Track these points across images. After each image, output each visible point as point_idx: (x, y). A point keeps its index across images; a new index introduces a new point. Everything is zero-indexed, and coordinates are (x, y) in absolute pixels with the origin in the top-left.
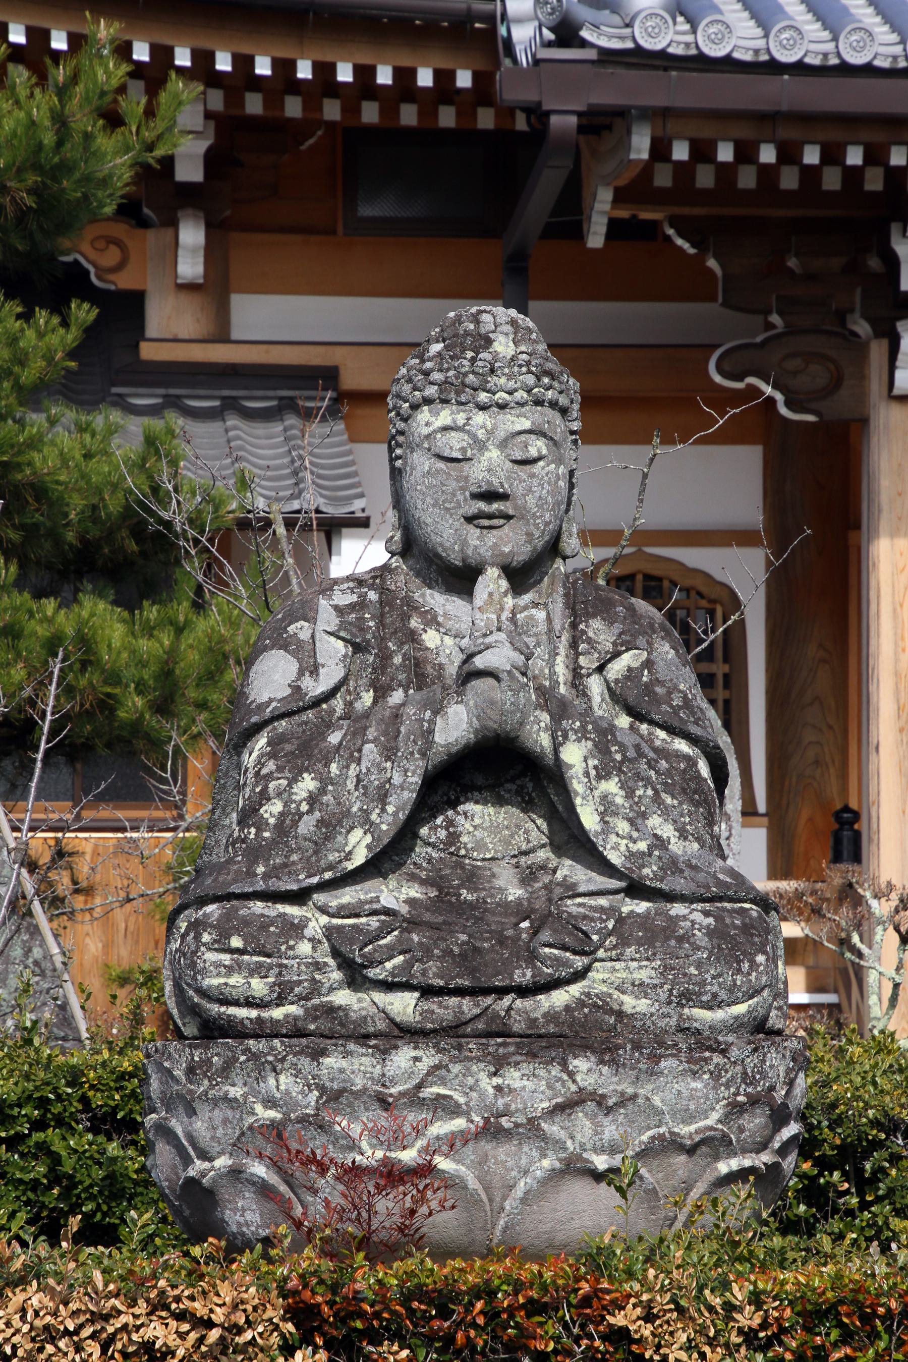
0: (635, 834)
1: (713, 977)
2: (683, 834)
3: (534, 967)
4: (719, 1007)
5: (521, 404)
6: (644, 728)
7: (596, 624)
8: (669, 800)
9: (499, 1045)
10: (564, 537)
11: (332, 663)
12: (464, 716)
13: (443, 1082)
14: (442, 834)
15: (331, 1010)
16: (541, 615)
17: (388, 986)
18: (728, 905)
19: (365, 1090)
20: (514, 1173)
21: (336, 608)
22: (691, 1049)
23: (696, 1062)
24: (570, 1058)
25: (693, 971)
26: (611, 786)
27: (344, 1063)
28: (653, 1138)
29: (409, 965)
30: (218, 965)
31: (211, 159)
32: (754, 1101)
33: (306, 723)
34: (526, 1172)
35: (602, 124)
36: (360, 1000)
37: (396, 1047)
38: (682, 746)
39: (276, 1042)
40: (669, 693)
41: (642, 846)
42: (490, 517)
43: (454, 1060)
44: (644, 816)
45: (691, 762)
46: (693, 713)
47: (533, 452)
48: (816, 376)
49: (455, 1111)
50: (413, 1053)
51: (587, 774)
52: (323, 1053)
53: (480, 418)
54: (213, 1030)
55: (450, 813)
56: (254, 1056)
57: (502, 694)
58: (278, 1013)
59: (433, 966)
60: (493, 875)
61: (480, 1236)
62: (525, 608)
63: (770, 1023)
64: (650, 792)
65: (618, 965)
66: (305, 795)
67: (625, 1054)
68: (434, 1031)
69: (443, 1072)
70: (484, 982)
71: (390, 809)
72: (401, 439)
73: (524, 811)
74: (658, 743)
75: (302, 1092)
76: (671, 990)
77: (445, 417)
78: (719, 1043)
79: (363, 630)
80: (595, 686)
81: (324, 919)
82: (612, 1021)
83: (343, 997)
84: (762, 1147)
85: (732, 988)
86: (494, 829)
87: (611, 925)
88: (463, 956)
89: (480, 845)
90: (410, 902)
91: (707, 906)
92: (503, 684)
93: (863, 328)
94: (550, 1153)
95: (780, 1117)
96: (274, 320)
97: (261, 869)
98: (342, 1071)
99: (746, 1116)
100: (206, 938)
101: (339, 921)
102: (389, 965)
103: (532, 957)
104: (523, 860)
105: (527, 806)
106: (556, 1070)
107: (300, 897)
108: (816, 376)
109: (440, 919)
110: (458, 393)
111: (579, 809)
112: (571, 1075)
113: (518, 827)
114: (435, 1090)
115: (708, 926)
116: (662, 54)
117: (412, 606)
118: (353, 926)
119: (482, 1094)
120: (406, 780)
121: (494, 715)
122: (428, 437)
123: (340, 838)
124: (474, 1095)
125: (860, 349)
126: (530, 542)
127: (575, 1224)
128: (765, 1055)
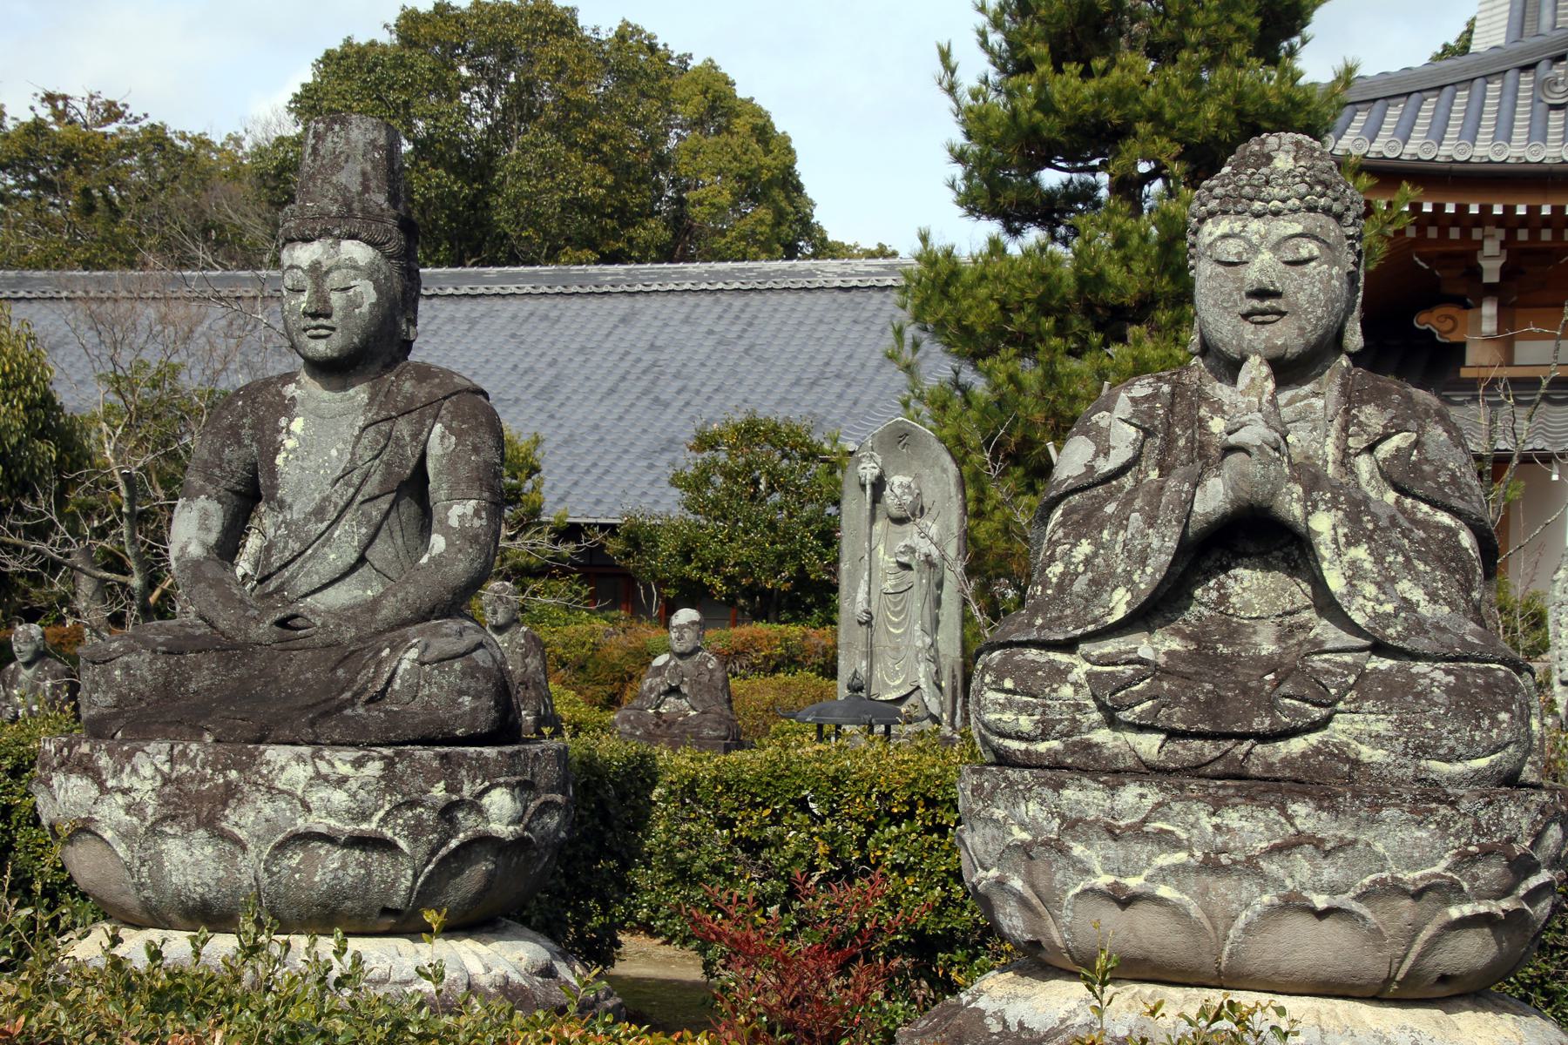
0: (1382, 597)
1: (1450, 732)
2: (1433, 597)
3: (1273, 715)
4: (1458, 760)
5: (1294, 211)
6: (1408, 502)
7: (1369, 409)
8: (1421, 567)
9: (1219, 787)
10: (1348, 335)
12: (1221, 488)
13: (1166, 818)
14: (1214, 595)
15: (1088, 746)
16: (1319, 403)
17: (1140, 728)
18: (1473, 665)
19: (1098, 820)
20: (1235, 906)
21: (1133, 400)
23: (1420, 813)
25: (1429, 725)
26: (1361, 553)
27: (1080, 795)
28: (1375, 882)
29: (1155, 711)
30: (995, 702)
31: (1504, 271)
32: (1487, 852)
33: (1095, 497)
34: (1247, 906)
36: (1115, 739)
37: (1124, 784)
38: (1444, 518)
39: (1027, 773)
40: (1437, 471)
42: (1263, 313)
43: (1176, 799)
44: (1394, 580)
45: (1452, 533)
46: (1459, 489)
47: (1304, 253)
49: (1177, 845)
50: (1140, 790)
51: (1335, 541)
52: (1063, 785)
53: (1255, 225)
54: (1004, 760)
55: (1222, 577)
56: (1011, 784)
57: (1254, 468)
58: (1042, 747)
59: (1178, 712)
60: (1255, 632)
61: (1209, 960)
62: (1306, 397)
63: (1523, 776)
64: (1400, 559)
65: (1357, 717)
66: (1082, 557)
68: (1176, 770)
69: (1165, 809)
71: (1149, 570)
72: (1192, 251)
73: (1290, 575)
74: (1420, 515)
75: (1046, 819)
76: (1406, 743)
77: (1224, 225)
78: (1448, 796)
80: (1364, 465)
81: (1087, 666)
82: (1346, 768)
83: (1103, 736)
84: (1506, 893)
86: (1261, 592)
87: (1351, 680)
88: (1208, 703)
89: (1247, 605)
90: (1171, 654)
91: (1451, 665)
92: (1254, 458)
94: (1270, 890)
96: (1537, 354)
97: (1039, 621)
98: (1078, 802)
99: (1480, 865)
100: (988, 679)
101: (1098, 669)
102: (1138, 709)
103: (1272, 707)
104: (1287, 620)
105: (1293, 570)
106: (1273, 814)
107: (1069, 646)
109: (1193, 670)
111: (1325, 573)
112: (1290, 818)
113: (1284, 590)
114: (1159, 825)
115: (1447, 685)
117: (1203, 398)
119: (1202, 831)
120: (1163, 544)
121: (1245, 487)
122: (1210, 245)
123: (1105, 596)
127: (1298, 956)
128: (1501, 808)
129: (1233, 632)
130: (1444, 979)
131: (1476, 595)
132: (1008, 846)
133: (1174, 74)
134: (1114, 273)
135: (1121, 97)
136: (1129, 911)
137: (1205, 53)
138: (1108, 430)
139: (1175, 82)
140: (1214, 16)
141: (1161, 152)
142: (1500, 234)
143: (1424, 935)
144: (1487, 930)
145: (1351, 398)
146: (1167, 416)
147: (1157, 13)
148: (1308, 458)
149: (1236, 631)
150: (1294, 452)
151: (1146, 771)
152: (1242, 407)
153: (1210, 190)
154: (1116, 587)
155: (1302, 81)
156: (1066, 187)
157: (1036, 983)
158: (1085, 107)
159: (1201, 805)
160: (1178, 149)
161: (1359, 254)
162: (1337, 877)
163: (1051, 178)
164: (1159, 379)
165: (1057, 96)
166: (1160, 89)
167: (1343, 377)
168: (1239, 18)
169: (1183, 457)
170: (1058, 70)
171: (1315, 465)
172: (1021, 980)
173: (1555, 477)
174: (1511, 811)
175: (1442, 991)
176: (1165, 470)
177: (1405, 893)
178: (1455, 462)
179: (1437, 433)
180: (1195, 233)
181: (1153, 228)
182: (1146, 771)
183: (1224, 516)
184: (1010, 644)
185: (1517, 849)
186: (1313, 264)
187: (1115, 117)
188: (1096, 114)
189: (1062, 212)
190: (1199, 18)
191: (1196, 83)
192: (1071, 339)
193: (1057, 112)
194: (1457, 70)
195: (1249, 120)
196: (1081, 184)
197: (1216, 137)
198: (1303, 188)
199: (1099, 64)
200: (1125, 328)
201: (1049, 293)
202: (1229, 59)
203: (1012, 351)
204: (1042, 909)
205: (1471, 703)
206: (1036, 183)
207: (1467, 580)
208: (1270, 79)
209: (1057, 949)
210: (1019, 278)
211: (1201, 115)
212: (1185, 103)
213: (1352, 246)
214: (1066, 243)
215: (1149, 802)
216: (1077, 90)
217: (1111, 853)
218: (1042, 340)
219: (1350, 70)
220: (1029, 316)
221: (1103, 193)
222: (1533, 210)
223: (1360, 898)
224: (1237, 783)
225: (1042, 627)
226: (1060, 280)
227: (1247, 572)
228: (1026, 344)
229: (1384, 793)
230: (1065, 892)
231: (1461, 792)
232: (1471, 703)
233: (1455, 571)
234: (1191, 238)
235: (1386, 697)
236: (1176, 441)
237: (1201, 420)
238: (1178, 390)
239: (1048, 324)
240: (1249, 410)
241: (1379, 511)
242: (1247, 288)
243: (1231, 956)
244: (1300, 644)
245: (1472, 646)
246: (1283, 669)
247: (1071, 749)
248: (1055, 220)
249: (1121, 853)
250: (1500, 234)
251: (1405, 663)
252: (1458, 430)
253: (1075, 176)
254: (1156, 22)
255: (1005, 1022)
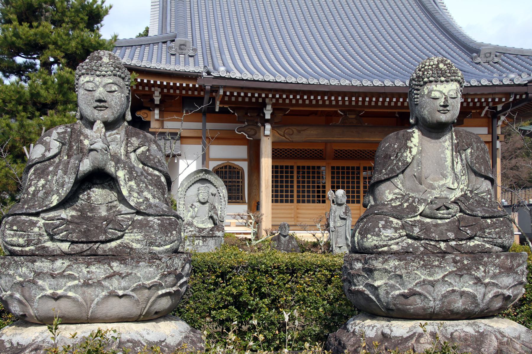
0: (139, 197)
2: (154, 197)
3: (106, 235)
6: (146, 168)
7: (134, 139)
8: (150, 187)
9: (89, 259)
10: (127, 115)
11: (54, 148)
12: (88, 163)
13: (71, 270)
14: (86, 197)
15: (44, 247)
16: (118, 136)
17: (62, 241)
18: (166, 217)
19: (47, 272)
21: (58, 133)
22: (150, 259)
23: (151, 263)
24: (111, 263)
25: (153, 236)
26: (132, 183)
27: (41, 264)
28: (137, 285)
29: (67, 235)
30: (10, 234)
31: (160, 100)
32: (170, 273)
34: (97, 296)
35: (215, 89)
36: (53, 245)
37: (57, 260)
38: (157, 173)
39: (22, 258)
41: (141, 200)
42: (101, 107)
43: (74, 263)
44: (142, 192)
45: (159, 177)
46: (161, 164)
47: (113, 89)
48: (252, 132)
50: (62, 261)
51: (125, 180)
52: (35, 261)
53: (97, 79)
54: (13, 254)
55: (89, 191)
56: (16, 262)
58: (27, 249)
59: (75, 235)
60: (99, 209)
61: (84, 315)
62: (114, 134)
64: (144, 185)
65: (132, 234)
66: (41, 185)
67: (129, 261)
68: (74, 254)
69: (71, 267)
70: (90, 239)
71: (65, 189)
72: (77, 86)
73: (110, 190)
74: (150, 172)
75: (29, 273)
77: (87, 78)
78: (159, 257)
79: (65, 139)
80: (133, 156)
81: (44, 221)
82: (129, 251)
83: (49, 244)
84: (174, 285)
85: (165, 241)
86: (101, 196)
87: (130, 223)
88: (85, 232)
89: (97, 200)
91: (159, 217)
93: (259, 124)
95: (179, 277)
96: (171, 125)
97: (26, 206)
98: (40, 267)
100: (7, 226)
101: (48, 222)
102: (61, 235)
103: (105, 232)
104: (110, 204)
105: (111, 189)
106: (106, 266)
107: (37, 214)
108: (252, 132)
109: (80, 221)
110: (91, 72)
111: (122, 190)
112: (111, 267)
113: (109, 195)
114: (69, 272)
116: (224, 77)
117: (81, 133)
118: (51, 223)
119: (83, 273)
120: (69, 181)
122: (83, 84)
123: (50, 198)
124: (81, 274)
125: (259, 128)
126: (113, 115)
127: (113, 310)
129: (92, 209)
130: (156, 313)
131: (166, 196)
132: (15, 283)
133: (61, 30)
134: (43, 92)
135: (43, 36)
136: (58, 301)
137: (71, 25)
138: (50, 142)
139: (61, 33)
140: (73, 14)
141: (58, 55)
142: (159, 90)
143: (151, 300)
144: (169, 297)
145: (128, 135)
146: (69, 139)
147: (54, 10)
148: (115, 153)
149: (93, 208)
150: (112, 151)
151: (64, 255)
152: (95, 137)
153: (82, 66)
154: (53, 195)
155: (102, 38)
156: (25, 63)
157: (23, 328)
158: (31, 37)
159: (83, 265)
160: (63, 54)
161: (129, 91)
162: (126, 285)
163: (20, 60)
164: (67, 127)
165: (21, 33)
166: (56, 35)
167: (126, 128)
168: (81, 15)
169: (75, 152)
170: (21, 24)
171: (118, 156)
172: (18, 328)
173: (176, 161)
174: (176, 261)
175: (156, 316)
176: (69, 156)
177: (146, 288)
178: (159, 155)
179: (154, 147)
180: (78, 80)
181: (56, 79)
182: (64, 255)
183: (90, 171)
184: (15, 214)
185: (178, 272)
186: (116, 93)
187: (41, 42)
188: (35, 40)
189: (24, 71)
190: (68, 14)
191: (68, 34)
192: (28, 113)
193: (21, 38)
194: (144, 40)
195: (86, 48)
196: (30, 63)
197: (75, 52)
198: (112, 69)
199: (35, 24)
200: (47, 111)
201: (21, 97)
202: (79, 28)
203: (8, 116)
204: (27, 303)
205: (165, 229)
206: (14, 61)
207: (163, 191)
208: (92, 36)
209: (31, 316)
210: (9, 92)
211: (70, 44)
212: (65, 40)
213: (128, 88)
214: (26, 82)
215: (65, 265)
216: (28, 32)
217: (52, 283)
218: (18, 113)
219: (116, 36)
220: (13, 105)
221: (38, 67)
222: (168, 84)
223: (132, 291)
224: (95, 257)
225: (27, 208)
226: (24, 93)
227: (97, 190)
228: (13, 114)
229: (140, 258)
230: (35, 297)
231: (162, 256)
232: (165, 229)
233: (160, 189)
234: (76, 81)
235: (140, 228)
236: (73, 147)
237: (81, 140)
238: (73, 130)
239: (20, 108)
240: (97, 138)
241: (138, 170)
242: (96, 99)
243: (92, 313)
244: (114, 212)
245: (165, 211)
246: (109, 220)
247: (37, 249)
248: (21, 74)
249: (56, 282)
250: (159, 90)
251: (146, 217)
252: (160, 146)
253: (28, 60)
254: (54, 13)
255: (12, 343)
